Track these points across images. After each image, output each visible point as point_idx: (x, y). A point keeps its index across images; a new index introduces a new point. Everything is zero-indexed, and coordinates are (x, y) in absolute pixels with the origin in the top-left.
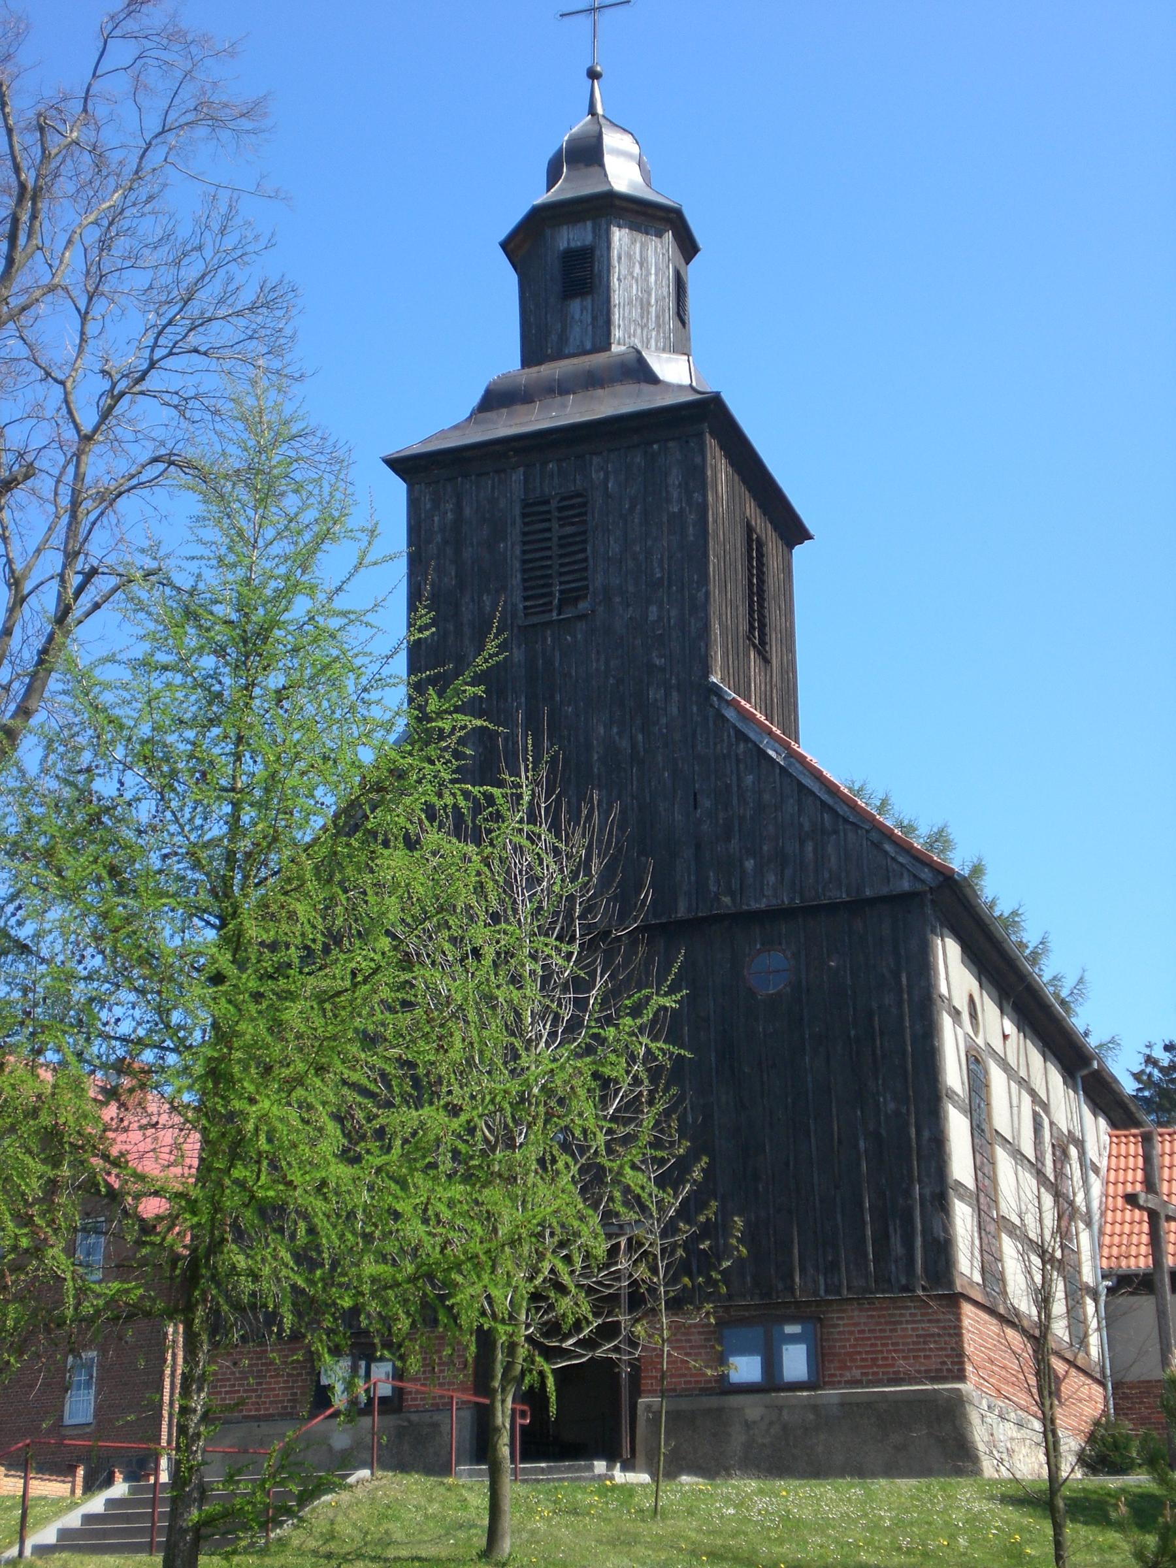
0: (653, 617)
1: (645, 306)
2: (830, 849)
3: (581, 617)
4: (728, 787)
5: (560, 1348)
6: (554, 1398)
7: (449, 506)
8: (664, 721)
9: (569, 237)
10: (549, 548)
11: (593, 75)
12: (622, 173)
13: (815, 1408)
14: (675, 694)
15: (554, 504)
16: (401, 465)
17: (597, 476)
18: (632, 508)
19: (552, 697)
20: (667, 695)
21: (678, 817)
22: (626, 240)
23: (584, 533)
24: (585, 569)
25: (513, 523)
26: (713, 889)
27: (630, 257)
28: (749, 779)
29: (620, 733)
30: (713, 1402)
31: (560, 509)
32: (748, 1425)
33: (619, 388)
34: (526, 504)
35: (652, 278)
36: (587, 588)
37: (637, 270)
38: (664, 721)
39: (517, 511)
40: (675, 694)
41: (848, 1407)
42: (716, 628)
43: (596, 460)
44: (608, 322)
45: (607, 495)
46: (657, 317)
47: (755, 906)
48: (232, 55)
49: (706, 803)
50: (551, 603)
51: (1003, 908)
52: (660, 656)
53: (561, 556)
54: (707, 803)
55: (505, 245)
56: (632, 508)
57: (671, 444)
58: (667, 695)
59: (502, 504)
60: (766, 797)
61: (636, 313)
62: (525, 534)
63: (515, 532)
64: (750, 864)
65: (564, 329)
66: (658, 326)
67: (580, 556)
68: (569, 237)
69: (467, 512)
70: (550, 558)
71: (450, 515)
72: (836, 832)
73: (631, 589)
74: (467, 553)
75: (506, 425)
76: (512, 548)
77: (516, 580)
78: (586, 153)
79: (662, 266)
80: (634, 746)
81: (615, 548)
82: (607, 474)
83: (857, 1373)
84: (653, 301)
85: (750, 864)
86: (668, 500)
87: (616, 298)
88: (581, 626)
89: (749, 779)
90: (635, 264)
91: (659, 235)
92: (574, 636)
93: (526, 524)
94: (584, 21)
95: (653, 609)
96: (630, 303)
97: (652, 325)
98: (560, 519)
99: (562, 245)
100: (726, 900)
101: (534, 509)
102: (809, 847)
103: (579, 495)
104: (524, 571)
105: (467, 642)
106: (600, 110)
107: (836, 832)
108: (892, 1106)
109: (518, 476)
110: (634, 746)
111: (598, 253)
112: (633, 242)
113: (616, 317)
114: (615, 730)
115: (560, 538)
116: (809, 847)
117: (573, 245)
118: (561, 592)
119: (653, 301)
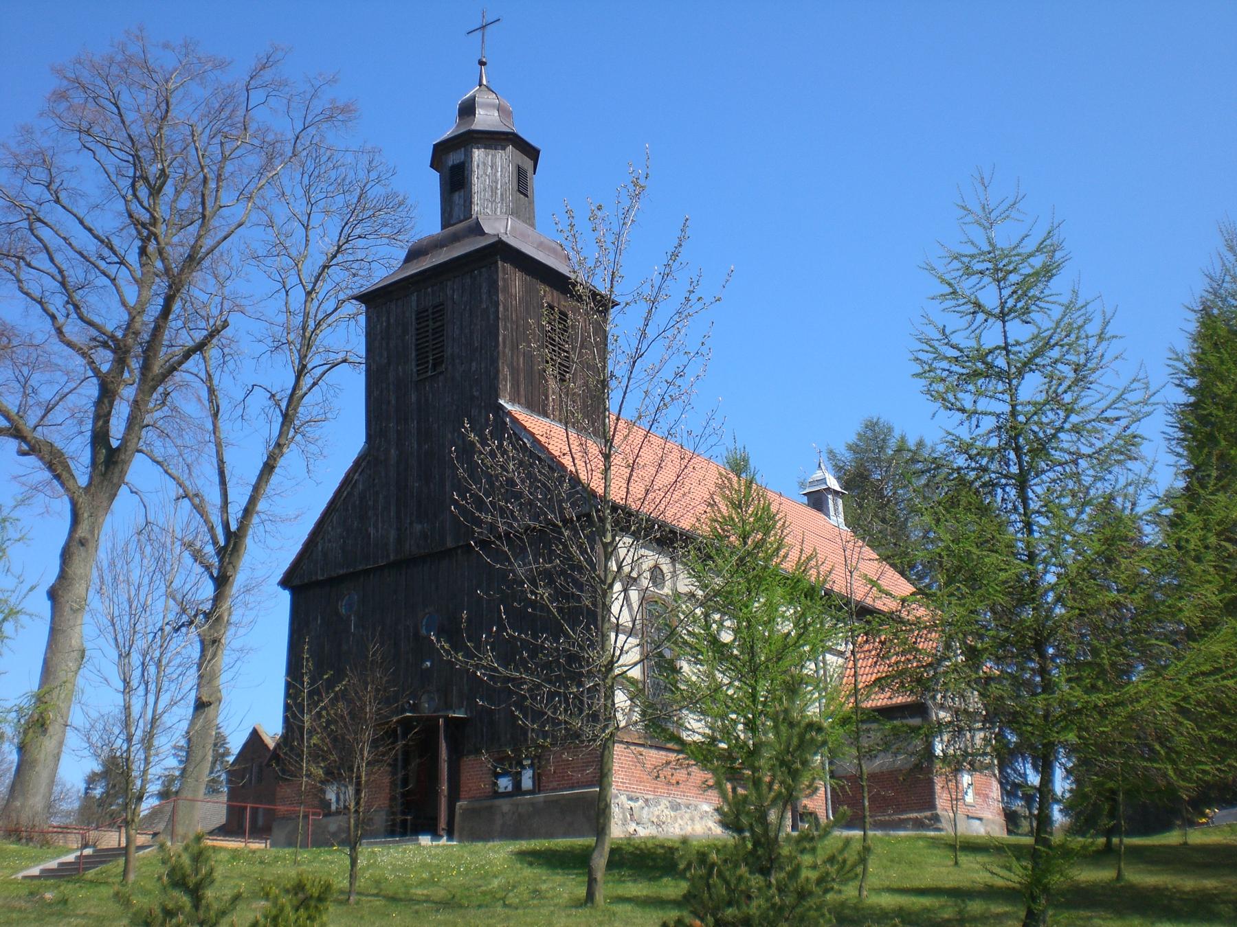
1: (494, 191)
3: (441, 373)
6: (446, 793)
9: (454, 158)
11: (482, 63)
12: (486, 119)
13: (532, 804)
16: (361, 298)
17: (449, 292)
20: (480, 412)
22: (482, 155)
27: (484, 164)
30: (487, 803)
32: (503, 815)
33: (467, 240)
34: (418, 313)
37: (489, 170)
41: (549, 803)
42: (505, 371)
43: (449, 283)
44: (471, 203)
48: (335, 82)
51: (1193, 316)
58: (480, 412)
66: (502, 200)
68: (454, 158)
69: (392, 321)
75: (413, 269)
76: (411, 338)
78: (468, 109)
83: (555, 784)
87: (475, 189)
88: (441, 378)
90: (489, 170)
91: (504, 148)
94: (478, 34)
95: (474, 364)
96: (485, 190)
99: (450, 163)
101: (421, 315)
104: (417, 350)
106: (484, 82)
109: (414, 297)
113: (475, 199)
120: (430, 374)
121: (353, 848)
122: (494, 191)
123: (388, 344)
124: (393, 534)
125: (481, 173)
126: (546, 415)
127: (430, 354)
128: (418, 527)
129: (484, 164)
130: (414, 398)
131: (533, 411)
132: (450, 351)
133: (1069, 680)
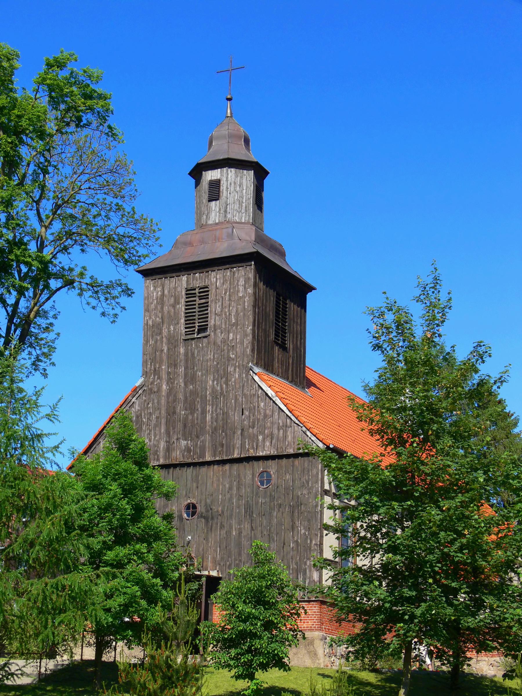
0: (231, 338)
1: (241, 204)
2: (289, 433)
4: (254, 407)
5: (16, 692)
7: (159, 289)
8: (233, 380)
10: (195, 308)
14: (237, 369)
15: (197, 291)
18: (225, 293)
19: (194, 368)
20: (235, 370)
21: (236, 418)
23: (208, 302)
24: (207, 317)
25: (182, 297)
26: (247, 447)
28: (262, 404)
29: (217, 384)
31: (200, 293)
35: (245, 191)
36: (207, 325)
37: (238, 189)
38: (233, 380)
39: (184, 293)
40: (237, 369)
45: (217, 288)
46: (246, 207)
47: (261, 454)
49: (247, 413)
50: (194, 330)
52: (233, 354)
53: (199, 312)
54: (247, 413)
55: (190, 174)
56: (225, 293)
57: (241, 268)
58: (235, 370)
59: (179, 289)
60: (268, 411)
61: (237, 206)
62: (186, 302)
63: (183, 301)
64: (260, 438)
65: (208, 213)
66: (246, 211)
67: (206, 312)
69: (166, 292)
70: (195, 312)
71: (159, 293)
72: (291, 427)
73: (223, 326)
74: (166, 309)
76: (182, 307)
77: (183, 321)
79: (249, 185)
80: (222, 388)
81: (219, 310)
82: (217, 279)
84: (244, 201)
85: (260, 438)
86: (238, 291)
88: (205, 340)
89: (262, 404)
92: (202, 344)
93: (187, 298)
94: (227, 74)
97: (243, 211)
98: (199, 296)
100: (252, 451)
101: (190, 292)
102: (281, 432)
103: (207, 287)
105: (164, 345)
107: (291, 427)
108: (303, 531)
110: (222, 388)
111: (222, 182)
112: (237, 176)
114: (215, 382)
115: (199, 304)
116: (281, 432)
117: (213, 179)
118: (199, 326)
119: (244, 201)
120: (195, 336)
121: (82, 659)
122: (241, 204)
123: (162, 308)
124: (162, 445)
125: (232, 189)
126: (272, 372)
127: (196, 322)
128: (183, 443)
129: (235, 183)
130: (182, 350)
131: (267, 370)
132: (212, 322)
133: (269, 561)
